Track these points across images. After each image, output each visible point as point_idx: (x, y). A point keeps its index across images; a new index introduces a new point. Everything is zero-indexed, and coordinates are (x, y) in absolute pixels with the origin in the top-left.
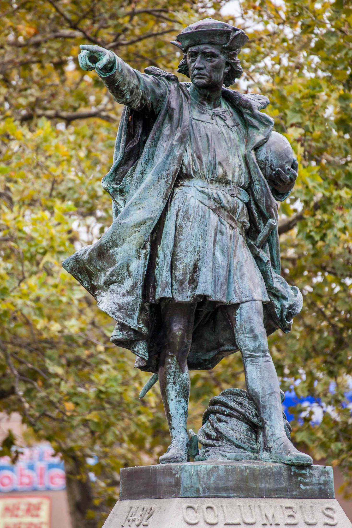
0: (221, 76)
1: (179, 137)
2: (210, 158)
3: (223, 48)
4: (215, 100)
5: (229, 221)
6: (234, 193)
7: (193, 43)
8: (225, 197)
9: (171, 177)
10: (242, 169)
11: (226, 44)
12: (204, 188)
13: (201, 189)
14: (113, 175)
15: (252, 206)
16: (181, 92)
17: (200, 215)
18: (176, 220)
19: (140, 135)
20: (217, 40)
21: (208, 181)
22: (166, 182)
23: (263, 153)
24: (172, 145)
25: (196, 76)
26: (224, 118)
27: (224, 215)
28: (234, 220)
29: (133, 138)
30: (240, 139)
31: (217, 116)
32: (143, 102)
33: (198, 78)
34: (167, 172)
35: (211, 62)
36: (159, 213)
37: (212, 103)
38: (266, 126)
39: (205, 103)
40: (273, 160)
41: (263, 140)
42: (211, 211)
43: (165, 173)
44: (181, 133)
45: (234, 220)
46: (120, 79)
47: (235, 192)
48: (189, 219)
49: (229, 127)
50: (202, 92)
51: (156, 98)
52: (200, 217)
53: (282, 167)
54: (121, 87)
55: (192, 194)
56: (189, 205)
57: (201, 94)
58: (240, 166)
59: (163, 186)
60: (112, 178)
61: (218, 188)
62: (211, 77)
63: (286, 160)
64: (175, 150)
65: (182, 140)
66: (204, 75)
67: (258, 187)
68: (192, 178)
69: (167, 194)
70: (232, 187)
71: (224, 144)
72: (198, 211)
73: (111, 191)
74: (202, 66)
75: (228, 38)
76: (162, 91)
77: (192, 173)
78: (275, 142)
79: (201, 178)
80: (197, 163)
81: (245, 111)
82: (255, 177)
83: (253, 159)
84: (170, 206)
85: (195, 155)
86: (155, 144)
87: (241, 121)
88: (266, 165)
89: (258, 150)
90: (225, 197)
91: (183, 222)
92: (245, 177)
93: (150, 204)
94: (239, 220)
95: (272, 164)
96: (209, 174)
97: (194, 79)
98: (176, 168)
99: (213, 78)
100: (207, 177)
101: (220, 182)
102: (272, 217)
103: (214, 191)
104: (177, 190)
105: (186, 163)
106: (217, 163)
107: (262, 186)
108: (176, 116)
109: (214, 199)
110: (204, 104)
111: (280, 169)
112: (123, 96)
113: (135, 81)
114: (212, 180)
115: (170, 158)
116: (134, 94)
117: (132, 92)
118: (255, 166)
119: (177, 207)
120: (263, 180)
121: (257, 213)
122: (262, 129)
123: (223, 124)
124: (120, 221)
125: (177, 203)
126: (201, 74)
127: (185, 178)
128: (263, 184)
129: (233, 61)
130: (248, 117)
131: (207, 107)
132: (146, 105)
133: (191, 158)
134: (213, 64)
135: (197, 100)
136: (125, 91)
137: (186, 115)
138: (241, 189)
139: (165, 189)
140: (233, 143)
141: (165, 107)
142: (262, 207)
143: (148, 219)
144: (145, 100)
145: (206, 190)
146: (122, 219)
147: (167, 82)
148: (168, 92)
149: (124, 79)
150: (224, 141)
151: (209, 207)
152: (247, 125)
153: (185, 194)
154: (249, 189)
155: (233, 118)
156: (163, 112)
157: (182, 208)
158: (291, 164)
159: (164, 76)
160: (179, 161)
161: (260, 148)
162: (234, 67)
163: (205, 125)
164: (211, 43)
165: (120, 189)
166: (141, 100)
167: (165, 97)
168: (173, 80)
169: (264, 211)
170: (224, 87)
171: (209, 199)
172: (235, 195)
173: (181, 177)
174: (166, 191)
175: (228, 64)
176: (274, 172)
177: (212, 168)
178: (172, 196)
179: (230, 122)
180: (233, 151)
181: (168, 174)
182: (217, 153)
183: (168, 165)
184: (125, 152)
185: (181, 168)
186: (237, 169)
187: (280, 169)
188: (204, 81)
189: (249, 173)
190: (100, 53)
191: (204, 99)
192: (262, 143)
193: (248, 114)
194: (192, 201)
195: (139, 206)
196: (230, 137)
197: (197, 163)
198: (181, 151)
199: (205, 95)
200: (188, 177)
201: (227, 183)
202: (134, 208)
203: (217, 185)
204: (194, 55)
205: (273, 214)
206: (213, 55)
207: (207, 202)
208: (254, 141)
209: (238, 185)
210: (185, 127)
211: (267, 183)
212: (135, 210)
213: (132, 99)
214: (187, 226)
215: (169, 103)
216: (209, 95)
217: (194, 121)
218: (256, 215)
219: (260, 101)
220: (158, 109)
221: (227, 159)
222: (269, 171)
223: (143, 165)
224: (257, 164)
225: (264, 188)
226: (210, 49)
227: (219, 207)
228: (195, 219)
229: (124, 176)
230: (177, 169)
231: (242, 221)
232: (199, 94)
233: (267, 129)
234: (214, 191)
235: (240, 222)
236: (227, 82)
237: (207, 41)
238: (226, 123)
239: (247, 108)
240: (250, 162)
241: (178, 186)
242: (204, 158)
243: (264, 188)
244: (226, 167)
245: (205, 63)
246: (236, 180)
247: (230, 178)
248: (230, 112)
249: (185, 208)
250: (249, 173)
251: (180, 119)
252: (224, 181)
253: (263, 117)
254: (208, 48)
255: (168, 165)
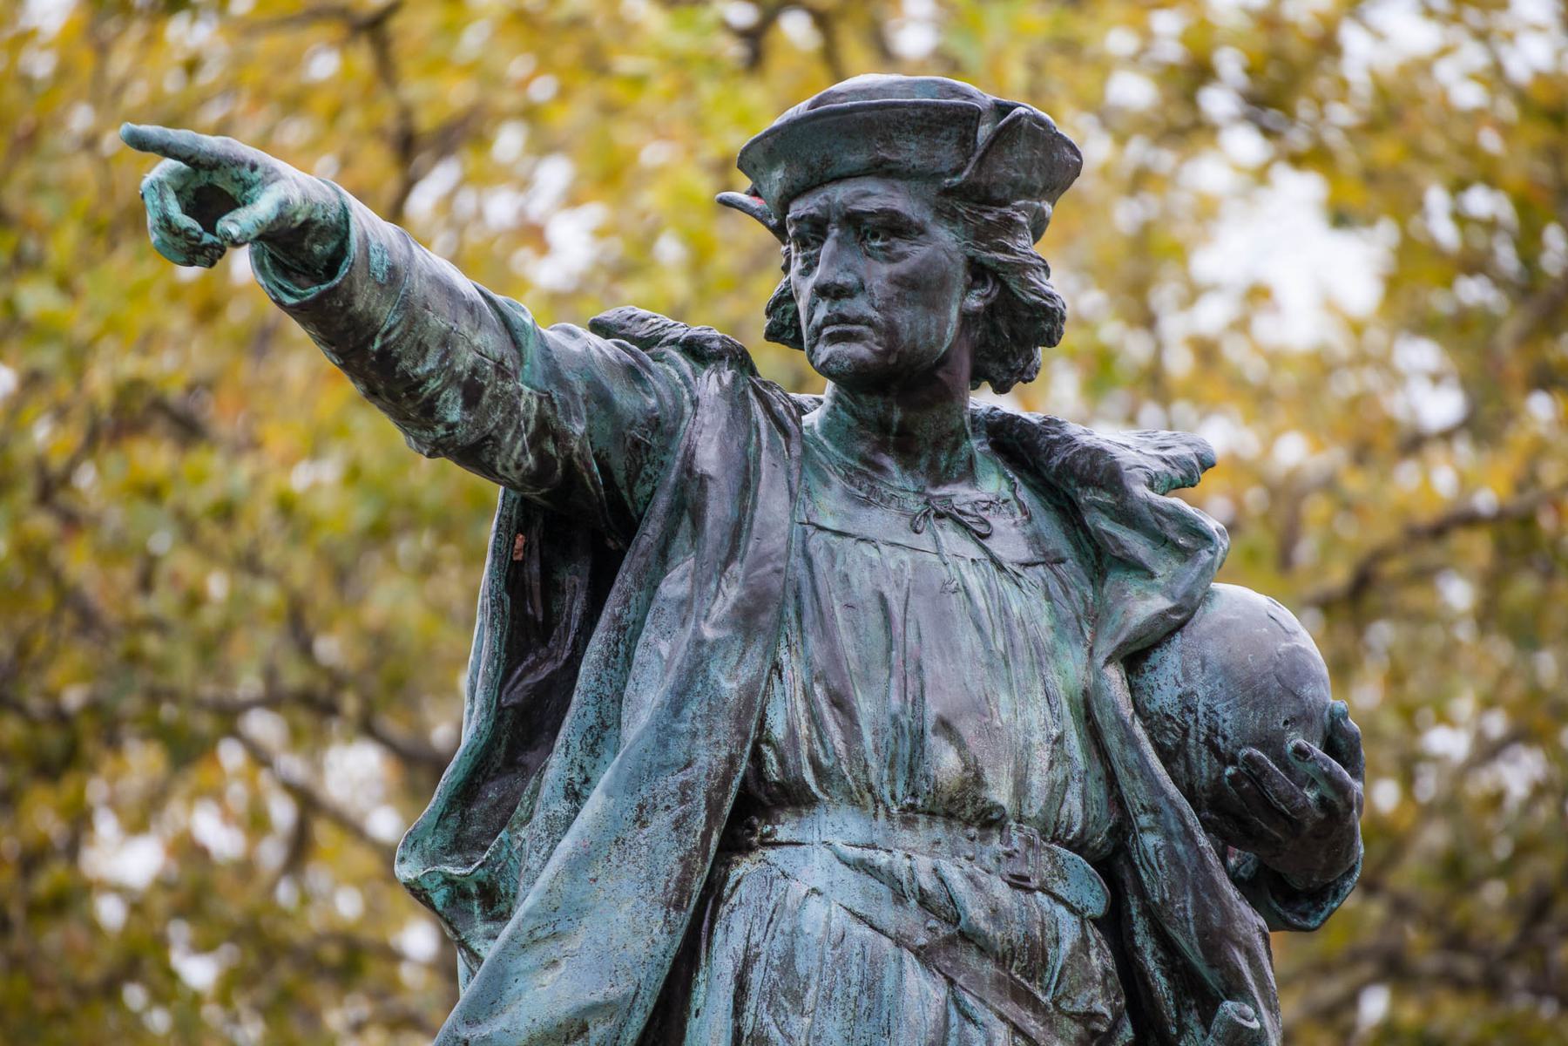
0: (944, 326)
1: (735, 607)
2: (895, 702)
3: (948, 192)
4: (937, 445)
5: (1009, 1008)
6: (1026, 870)
7: (802, 175)
8: (978, 886)
9: (701, 797)
10: (1068, 759)
11: (957, 171)
12: (873, 846)
13: (855, 853)
14: (452, 823)
15: (1139, 941)
16: (757, 408)
17: (855, 977)
18: (738, 1011)
19: (575, 624)
20: (910, 152)
21: (889, 816)
22: (678, 825)
23: (1169, 676)
24: (700, 642)
25: (826, 331)
26: (982, 529)
27: (976, 978)
28: (1035, 1005)
29: (544, 641)
30: (1059, 627)
31: (939, 516)
32: (550, 447)
33: (833, 339)
34: (681, 777)
35: (890, 260)
36: (654, 981)
37: (923, 462)
38: (1185, 554)
39: (887, 461)
40: (1220, 707)
41: (1162, 616)
42: (909, 957)
43: (674, 781)
44: (746, 585)
45: (1035, 1005)
46: (388, 316)
47: (1037, 867)
48: (797, 999)
49: (1001, 568)
50: (868, 413)
51: (619, 436)
52: (854, 991)
53: (1271, 743)
54: (405, 364)
55: (812, 881)
56: (795, 932)
57: (862, 421)
58: (1059, 740)
59: (664, 846)
60: (449, 836)
61: (944, 848)
62: (891, 331)
63: (1289, 708)
64: (713, 670)
65: (747, 619)
66: (857, 321)
67: (1151, 841)
68: (812, 801)
69: (683, 884)
70: (1016, 844)
71: (968, 639)
72: (843, 960)
73: (439, 898)
74: (848, 279)
75: (966, 141)
76: (652, 402)
77: (809, 776)
78: (1226, 625)
79: (853, 803)
80: (832, 726)
81: (1087, 496)
82: (1136, 793)
83: (1115, 705)
84: (709, 944)
85: (819, 690)
86: (622, 658)
87: (1078, 546)
88: (1186, 732)
89: (1146, 666)
90: (978, 886)
91: (767, 1019)
92: (1084, 795)
93: (602, 939)
94: (1065, 1005)
95: (1213, 730)
96: (893, 780)
97: (820, 348)
98: (724, 753)
99: (905, 337)
100: (886, 792)
101: (949, 816)
102: (1236, 989)
103: (924, 863)
104: (744, 868)
105: (778, 731)
106: (929, 725)
107: (1168, 835)
108: (718, 509)
109: (924, 900)
110: (881, 469)
111: (1257, 753)
112: (429, 410)
113: (489, 340)
114: (912, 807)
115: (693, 708)
116: (485, 400)
117: (472, 394)
118: (1130, 740)
119: (737, 943)
120: (1171, 803)
121: (1168, 977)
122: (1165, 567)
123: (972, 550)
124: (464, 1033)
125: (739, 928)
126: (843, 319)
127: (781, 806)
128: (1174, 827)
129: (1001, 256)
130: (1105, 525)
131: (897, 478)
132: (569, 464)
133: (801, 706)
134: (901, 268)
135: (848, 453)
136: (433, 384)
137: (773, 504)
138: (1064, 851)
139: (674, 857)
140: (1020, 637)
141: (673, 478)
142: (1182, 941)
143: (594, 1008)
144: (560, 437)
145: (882, 859)
146: (471, 1020)
147: (685, 365)
148: (689, 409)
149: (413, 320)
150: (971, 627)
151: (899, 941)
152: (1102, 561)
153: (782, 883)
154: (1113, 860)
155: (1029, 530)
156: (662, 501)
157: (764, 947)
158: (1318, 729)
159: (673, 342)
160: (740, 720)
161: (1155, 657)
162: (1014, 286)
163: (874, 555)
164: (882, 170)
165: (480, 884)
166: (535, 442)
167: (672, 434)
168: (718, 356)
169: (1197, 959)
170: (983, 400)
171: (900, 898)
172: (1035, 883)
173: (754, 805)
174: (678, 870)
175: (979, 272)
176: (1230, 770)
177: (905, 748)
178: (714, 892)
179: (1010, 542)
180: (1020, 671)
181: (685, 787)
182: (928, 678)
183: (685, 742)
184: (500, 708)
185: (757, 756)
186: (1041, 758)
187: (1257, 753)
188: (860, 350)
189: (1111, 780)
190: (245, 172)
191: (882, 447)
192: (1161, 628)
193: (1103, 508)
194: (816, 911)
195: (552, 950)
196: (1004, 611)
197: (832, 726)
198: (746, 673)
199: (883, 426)
200: (795, 798)
201: (989, 821)
202: (526, 961)
203: (939, 830)
204: (812, 232)
205: (1239, 974)
206: (895, 227)
207: (888, 915)
208: (1120, 620)
209: (1053, 832)
210: (762, 560)
211: (1193, 821)
212: (532, 970)
213: (478, 425)
214: (790, 1038)
215: (690, 456)
216: (902, 424)
217: (817, 541)
218: (1161, 983)
219: (1165, 453)
220: (641, 491)
221: (981, 708)
222: (1205, 767)
223: (577, 753)
224: (1138, 729)
225: (1180, 847)
226: (877, 197)
227: (950, 939)
228: (828, 998)
229: (503, 824)
230: (732, 761)
231: (1080, 1007)
232: (854, 423)
233: (1186, 567)
234: (924, 863)
235: (1071, 1015)
236: (994, 367)
237: (859, 158)
238: (985, 549)
239: (1100, 486)
240: (1105, 719)
241: (748, 849)
242: (865, 706)
243: (1180, 847)
244: (975, 745)
245: (862, 265)
246: (1036, 805)
247: (1000, 793)
248: (1021, 505)
249: (779, 945)
250: (1111, 780)
251: (738, 531)
252: (969, 812)
253: (1168, 515)
254: (867, 195)
255: (685, 742)
